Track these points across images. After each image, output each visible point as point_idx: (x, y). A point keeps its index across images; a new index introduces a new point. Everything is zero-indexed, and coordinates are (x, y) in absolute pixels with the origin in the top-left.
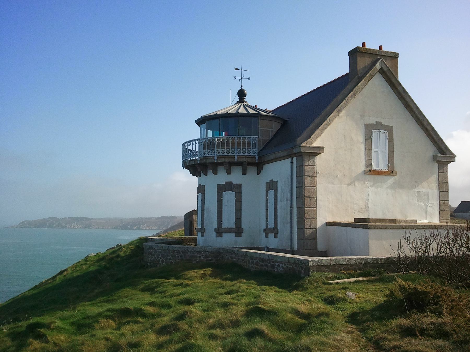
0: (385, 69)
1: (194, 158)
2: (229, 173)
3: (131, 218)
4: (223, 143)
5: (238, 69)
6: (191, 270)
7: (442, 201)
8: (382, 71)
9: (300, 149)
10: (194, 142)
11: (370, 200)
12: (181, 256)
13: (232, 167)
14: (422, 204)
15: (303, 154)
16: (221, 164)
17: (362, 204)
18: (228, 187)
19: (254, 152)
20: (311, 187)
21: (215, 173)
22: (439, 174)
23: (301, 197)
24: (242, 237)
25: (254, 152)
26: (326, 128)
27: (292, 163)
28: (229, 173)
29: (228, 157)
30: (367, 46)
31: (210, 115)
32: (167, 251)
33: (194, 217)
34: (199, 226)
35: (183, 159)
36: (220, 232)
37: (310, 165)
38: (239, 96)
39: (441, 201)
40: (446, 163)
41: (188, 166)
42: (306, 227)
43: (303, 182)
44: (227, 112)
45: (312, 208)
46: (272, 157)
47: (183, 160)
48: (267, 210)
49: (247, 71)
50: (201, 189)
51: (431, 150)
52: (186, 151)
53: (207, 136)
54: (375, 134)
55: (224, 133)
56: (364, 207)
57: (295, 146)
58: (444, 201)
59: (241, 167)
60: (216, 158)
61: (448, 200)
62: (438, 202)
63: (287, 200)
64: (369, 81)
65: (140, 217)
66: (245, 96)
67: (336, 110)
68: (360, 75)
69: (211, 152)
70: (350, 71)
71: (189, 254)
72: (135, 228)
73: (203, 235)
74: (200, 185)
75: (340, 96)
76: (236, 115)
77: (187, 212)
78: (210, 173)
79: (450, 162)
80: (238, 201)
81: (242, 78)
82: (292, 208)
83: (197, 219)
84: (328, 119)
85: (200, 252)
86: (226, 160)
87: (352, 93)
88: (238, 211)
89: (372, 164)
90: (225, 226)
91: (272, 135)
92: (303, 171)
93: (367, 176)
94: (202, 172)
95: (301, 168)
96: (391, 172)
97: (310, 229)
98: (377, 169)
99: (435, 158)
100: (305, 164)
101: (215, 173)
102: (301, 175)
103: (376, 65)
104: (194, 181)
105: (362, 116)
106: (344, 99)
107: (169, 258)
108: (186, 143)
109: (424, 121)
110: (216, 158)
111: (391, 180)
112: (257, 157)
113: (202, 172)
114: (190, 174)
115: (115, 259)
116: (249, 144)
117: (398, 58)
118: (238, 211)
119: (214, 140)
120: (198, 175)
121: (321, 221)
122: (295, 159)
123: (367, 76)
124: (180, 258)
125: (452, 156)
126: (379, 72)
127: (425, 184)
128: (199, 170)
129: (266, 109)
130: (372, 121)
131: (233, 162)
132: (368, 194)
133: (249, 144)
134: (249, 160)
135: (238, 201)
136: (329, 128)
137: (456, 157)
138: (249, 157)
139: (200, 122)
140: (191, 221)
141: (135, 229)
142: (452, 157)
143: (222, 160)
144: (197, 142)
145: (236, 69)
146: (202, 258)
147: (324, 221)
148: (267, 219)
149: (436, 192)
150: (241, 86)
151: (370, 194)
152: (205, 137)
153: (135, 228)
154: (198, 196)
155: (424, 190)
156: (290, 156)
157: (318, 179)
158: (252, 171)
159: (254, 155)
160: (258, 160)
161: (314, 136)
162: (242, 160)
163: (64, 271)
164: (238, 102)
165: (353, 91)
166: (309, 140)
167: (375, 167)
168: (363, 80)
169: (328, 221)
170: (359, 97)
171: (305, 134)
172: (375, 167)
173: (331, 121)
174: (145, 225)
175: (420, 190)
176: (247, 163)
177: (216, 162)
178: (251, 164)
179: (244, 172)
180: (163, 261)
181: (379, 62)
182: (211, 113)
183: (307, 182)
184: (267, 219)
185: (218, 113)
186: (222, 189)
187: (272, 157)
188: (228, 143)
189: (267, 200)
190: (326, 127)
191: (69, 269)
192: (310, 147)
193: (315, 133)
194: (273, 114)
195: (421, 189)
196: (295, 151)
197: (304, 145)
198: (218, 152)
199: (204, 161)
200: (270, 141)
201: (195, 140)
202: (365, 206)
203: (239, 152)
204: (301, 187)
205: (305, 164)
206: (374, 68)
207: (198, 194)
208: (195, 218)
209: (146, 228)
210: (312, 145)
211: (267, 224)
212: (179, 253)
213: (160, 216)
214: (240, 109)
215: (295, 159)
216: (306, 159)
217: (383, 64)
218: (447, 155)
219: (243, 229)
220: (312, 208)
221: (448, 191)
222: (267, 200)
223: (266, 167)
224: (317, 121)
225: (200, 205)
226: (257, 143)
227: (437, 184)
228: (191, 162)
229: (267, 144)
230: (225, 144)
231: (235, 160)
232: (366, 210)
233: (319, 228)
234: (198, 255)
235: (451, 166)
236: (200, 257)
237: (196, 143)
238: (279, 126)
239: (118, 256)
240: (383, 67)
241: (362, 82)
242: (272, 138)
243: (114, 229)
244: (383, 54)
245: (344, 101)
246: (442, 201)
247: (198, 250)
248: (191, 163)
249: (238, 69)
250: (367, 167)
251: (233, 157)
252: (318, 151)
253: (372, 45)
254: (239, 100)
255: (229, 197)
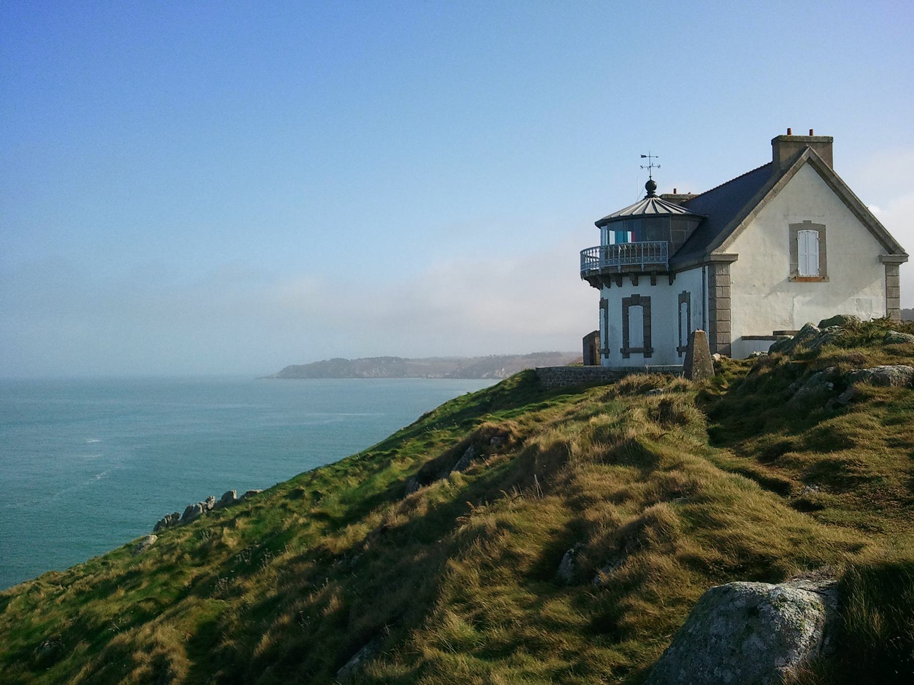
0: (814, 159)
1: (594, 269)
2: (635, 284)
3: (476, 358)
4: (628, 251)
5: (645, 156)
6: (596, 386)
7: (891, 309)
8: (810, 161)
9: (710, 258)
10: (594, 250)
11: (795, 311)
12: (584, 377)
13: (640, 277)
14: (863, 314)
15: (714, 263)
16: (626, 274)
17: (785, 316)
18: (636, 300)
19: (663, 260)
20: (723, 298)
21: (620, 285)
22: (886, 278)
23: (713, 309)
24: (652, 358)
25: (663, 260)
26: (740, 234)
27: (704, 272)
28: (635, 284)
29: (634, 266)
30: (793, 134)
31: (612, 217)
32: (568, 373)
33: (596, 341)
34: (603, 347)
35: (581, 269)
36: (626, 352)
37: (722, 275)
38: (647, 189)
39: (889, 309)
40: (896, 264)
41: (588, 277)
42: (718, 342)
43: (715, 294)
44: (632, 214)
45: (725, 321)
46: (683, 265)
47: (582, 270)
48: (680, 326)
49: (657, 157)
50: (604, 304)
51: (875, 249)
52: (584, 255)
53: (609, 243)
54: (802, 235)
55: (629, 233)
56: (788, 319)
57: (705, 255)
58: (893, 309)
59: (650, 277)
60: (619, 268)
61: (898, 308)
62: (885, 311)
63: (700, 314)
64: (793, 176)
65: (492, 355)
66: (655, 188)
67: (752, 212)
68: (783, 169)
69: (614, 261)
70: (773, 158)
71: (592, 375)
72: (485, 376)
73: (607, 357)
74: (602, 299)
75: (758, 195)
76: (643, 216)
77: (586, 335)
78: (614, 285)
79: (902, 263)
80: (647, 316)
81: (650, 167)
82: (704, 322)
83: (600, 343)
84: (743, 223)
85: (604, 372)
86: (632, 270)
87: (771, 191)
88: (647, 327)
89: (797, 270)
90: (632, 345)
91: (686, 237)
92: (715, 281)
93: (792, 283)
94: (604, 284)
95: (712, 277)
96: (823, 277)
97: (723, 344)
98: (805, 275)
99: (880, 259)
100: (717, 274)
101: (620, 285)
102: (713, 286)
103: (803, 155)
104: (595, 294)
105: (786, 216)
106: (763, 198)
107: (570, 380)
108: (584, 251)
109: (865, 216)
110: (619, 268)
111: (821, 285)
112: (667, 266)
113: (604, 284)
114: (591, 286)
115: (500, 392)
116: (658, 249)
117: (832, 143)
118: (647, 327)
119: (617, 248)
120: (600, 287)
121: (735, 336)
122: (707, 267)
123: (790, 169)
124: (582, 379)
125: (904, 255)
126: (807, 163)
127: (866, 290)
128: (600, 282)
129: (689, 193)
130: (799, 220)
131: (639, 272)
132: (793, 304)
133: (658, 249)
134: (658, 269)
135: (647, 316)
136: (745, 232)
137: (909, 256)
138: (658, 265)
139: (600, 224)
140: (592, 347)
141: (485, 378)
142: (904, 257)
143: (627, 270)
144: (598, 250)
145: (643, 156)
146: (606, 379)
147: (740, 336)
148: (680, 335)
149: (882, 298)
150: (650, 177)
151: (796, 303)
152: (607, 244)
153: (485, 376)
154: (600, 312)
155: (866, 297)
156: (701, 264)
157: (732, 290)
158: (663, 281)
159: (663, 262)
160: (669, 268)
161: (727, 243)
162: (649, 269)
163: (431, 413)
164: (646, 197)
165: (774, 188)
166: (719, 248)
167: (801, 274)
168: (786, 175)
169: (744, 335)
170: (782, 193)
171: (716, 241)
172: (801, 274)
173: (747, 225)
174: (503, 370)
175: (861, 298)
176: (656, 273)
177: (619, 272)
178: (660, 273)
179: (653, 283)
180: (563, 384)
181: (806, 152)
182: (613, 214)
183: (719, 293)
184: (680, 335)
185: (621, 215)
186: (627, 303)
187: (683, 265)
188: (633, 250)
189: (680, 314)
190: (740, 232)
191: (437, 411)
192: (721, 255)
193: (727, 240)
194: (688, 212)
195: (862, 297)
196: (706, 259)
197: (714, 253)
198: (622, 261)
199: (605, 272)
200: (684, 245)
201: (596, 248)
202: (790, 318)
203: (646, 260)
204: (713, 299)
205: (717, 274)
206: (799, 160)
207: (600, 309)
208: (598, 342)
209: (504, 375)
210: (724, 252)
211: (680, 341)
212: (582, 374)
213: (531, 353)
214: (647, 209)
215: (707, 267)
216: (717, 268)
217: (811, 153)
218: (896, 255)
219: (653, 348)
220: (725, 321)
221: (899, 298)
222: (680, 314)
223: (678, 275)
224: (730, 225)
225: (603, 323)
226: (667, 249)
227: (884, 290)
228: (591, 273)
229: (681, 249)
230: (631, 251)
231: (641, 270)
232: (791, 322)
233: (733, 342)
234: (602, 376)
235: (902, 267)
236: (604, 377)
237: (596, 251)
238: (696, 225)
239: (503, 389)
240: (811, 157)
241: (784, 177)
242: (687, 242)
243: (448, 377)
244: (812, 141)
245: (762, 201)
246: (891, 309)
247: (602, 370)
248: (591, 274)
249: (645, 156)
250: (791, 273)
251: (640, 266)
252: (730, 260)
253: (800, 131)
254: (647, 194)
255: (636, 312)
